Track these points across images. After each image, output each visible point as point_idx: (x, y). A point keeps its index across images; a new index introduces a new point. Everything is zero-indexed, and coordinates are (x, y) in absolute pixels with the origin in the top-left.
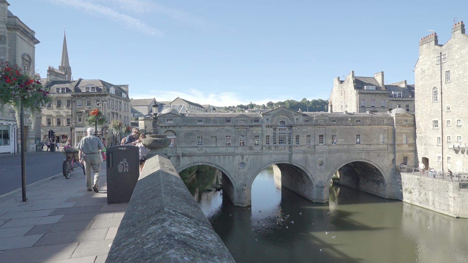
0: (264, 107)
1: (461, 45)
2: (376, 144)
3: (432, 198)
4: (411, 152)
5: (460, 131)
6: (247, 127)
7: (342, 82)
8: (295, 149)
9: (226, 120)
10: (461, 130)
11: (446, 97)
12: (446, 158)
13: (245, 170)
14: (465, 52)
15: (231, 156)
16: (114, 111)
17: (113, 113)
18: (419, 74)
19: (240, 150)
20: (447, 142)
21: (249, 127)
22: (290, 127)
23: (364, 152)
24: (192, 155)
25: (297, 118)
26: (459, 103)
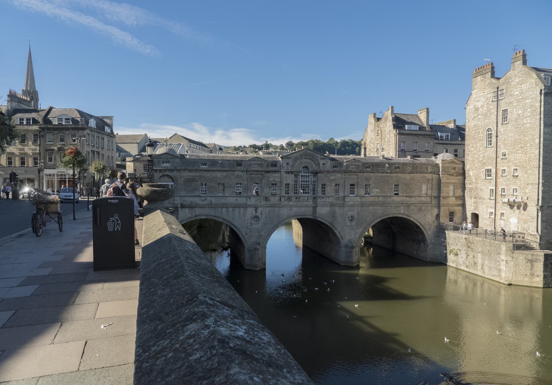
1: (521, 79)
2: (418, 196)
3: (482, 261)
4: (459, 206)
7: (378, 119)
8: (321, 201)
10: (518, 181)
11: (502, 141)
12: (498, 214)
13: (259, 225)
14: (526, 87)
16: (95, 149)
17: (93, 152)
18: (471, 112)
20: (501, 195)
21: (264, 173)
26: (517, 149)
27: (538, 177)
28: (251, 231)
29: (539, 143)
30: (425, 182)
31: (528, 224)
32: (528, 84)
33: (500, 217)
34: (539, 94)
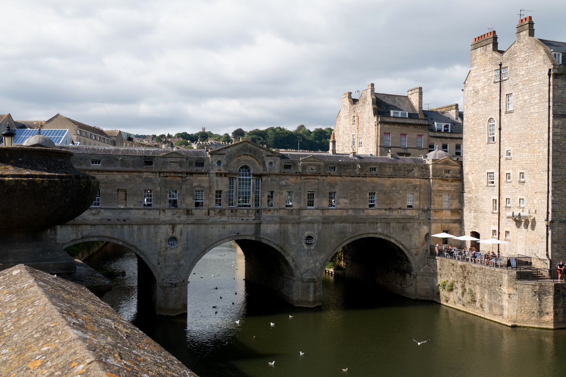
0: (227, 138)
1: (527, 54)
3: (480, 296)
4: (455, 223)
5: (523, 191)
6: (182, 174)
7: (355, 101)
8: (266, 215)
9: (145, 162)
10: (524, 189)
11: (506, 136)
13: (177, 250)
15: (152, 225)
18: (469, 95)
19: (168, 215)
20: (506, 207)
21: (186, 176)
22: (259, 176)
23: (381, 222)
24: (79, 223)
25: (270, 161)
26: (523, 146)
27: (547, 183)
28: (165, 259)
29: (547, 139)
30: (411, 189)
31: (537, 246)
32: (535, 62)
33: (504, 237)
34: (547, 75)
